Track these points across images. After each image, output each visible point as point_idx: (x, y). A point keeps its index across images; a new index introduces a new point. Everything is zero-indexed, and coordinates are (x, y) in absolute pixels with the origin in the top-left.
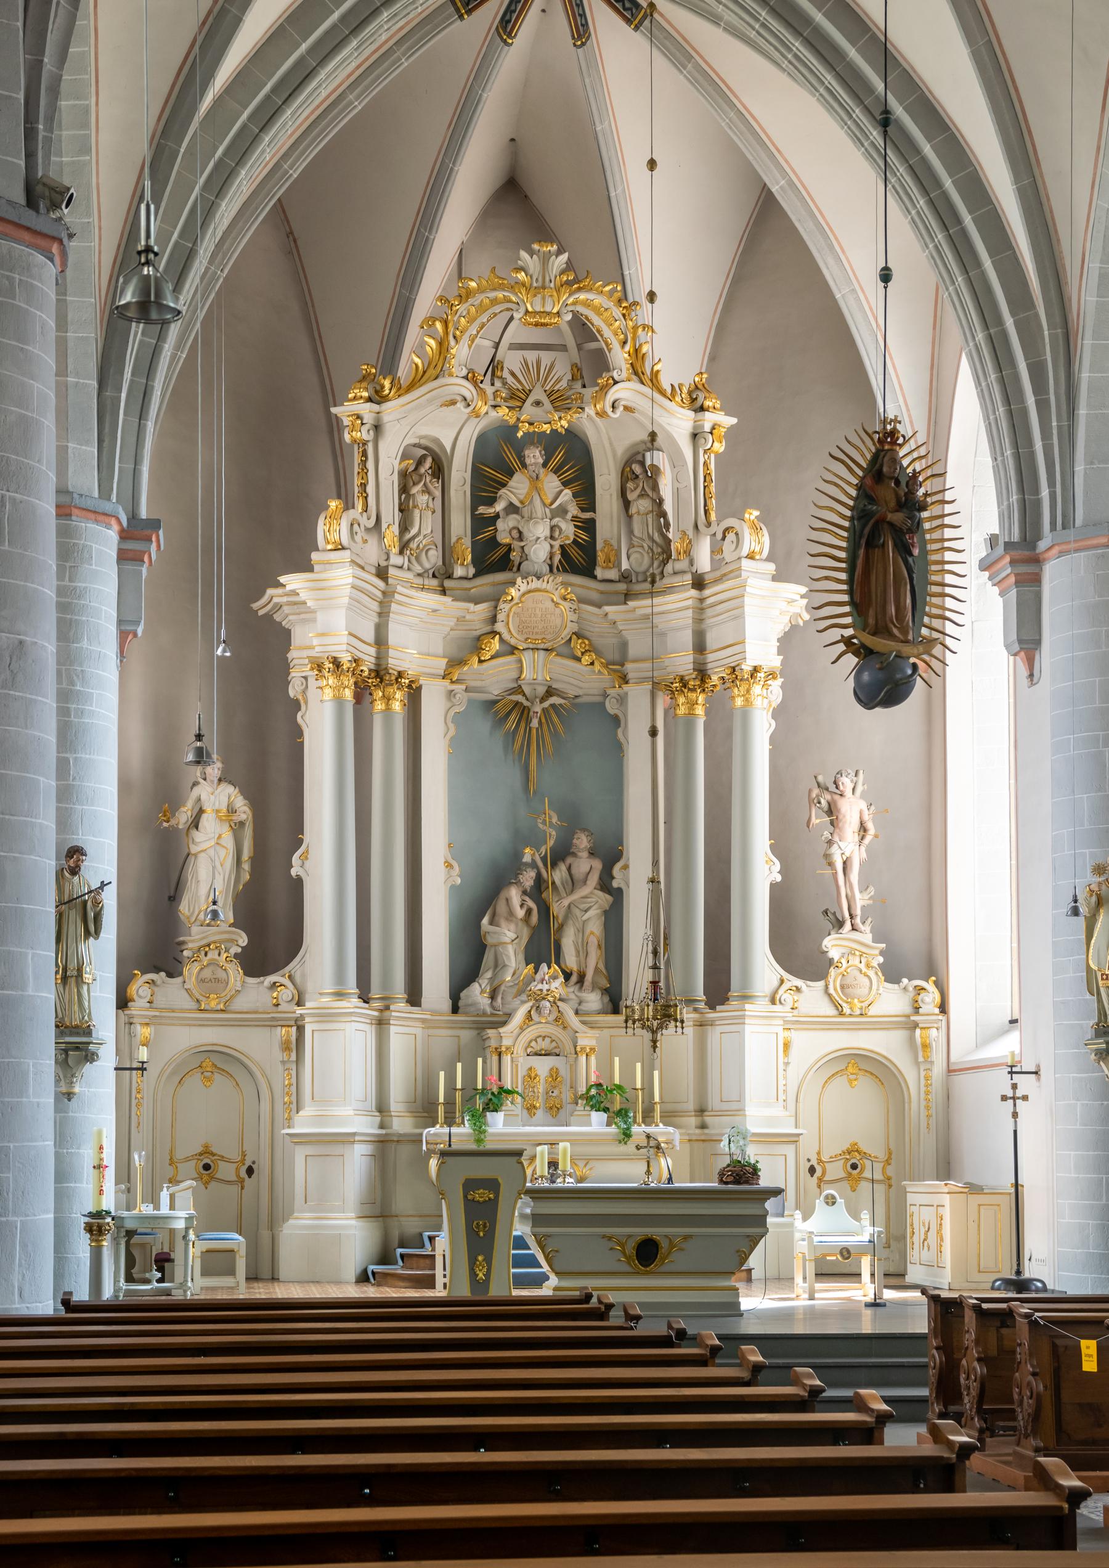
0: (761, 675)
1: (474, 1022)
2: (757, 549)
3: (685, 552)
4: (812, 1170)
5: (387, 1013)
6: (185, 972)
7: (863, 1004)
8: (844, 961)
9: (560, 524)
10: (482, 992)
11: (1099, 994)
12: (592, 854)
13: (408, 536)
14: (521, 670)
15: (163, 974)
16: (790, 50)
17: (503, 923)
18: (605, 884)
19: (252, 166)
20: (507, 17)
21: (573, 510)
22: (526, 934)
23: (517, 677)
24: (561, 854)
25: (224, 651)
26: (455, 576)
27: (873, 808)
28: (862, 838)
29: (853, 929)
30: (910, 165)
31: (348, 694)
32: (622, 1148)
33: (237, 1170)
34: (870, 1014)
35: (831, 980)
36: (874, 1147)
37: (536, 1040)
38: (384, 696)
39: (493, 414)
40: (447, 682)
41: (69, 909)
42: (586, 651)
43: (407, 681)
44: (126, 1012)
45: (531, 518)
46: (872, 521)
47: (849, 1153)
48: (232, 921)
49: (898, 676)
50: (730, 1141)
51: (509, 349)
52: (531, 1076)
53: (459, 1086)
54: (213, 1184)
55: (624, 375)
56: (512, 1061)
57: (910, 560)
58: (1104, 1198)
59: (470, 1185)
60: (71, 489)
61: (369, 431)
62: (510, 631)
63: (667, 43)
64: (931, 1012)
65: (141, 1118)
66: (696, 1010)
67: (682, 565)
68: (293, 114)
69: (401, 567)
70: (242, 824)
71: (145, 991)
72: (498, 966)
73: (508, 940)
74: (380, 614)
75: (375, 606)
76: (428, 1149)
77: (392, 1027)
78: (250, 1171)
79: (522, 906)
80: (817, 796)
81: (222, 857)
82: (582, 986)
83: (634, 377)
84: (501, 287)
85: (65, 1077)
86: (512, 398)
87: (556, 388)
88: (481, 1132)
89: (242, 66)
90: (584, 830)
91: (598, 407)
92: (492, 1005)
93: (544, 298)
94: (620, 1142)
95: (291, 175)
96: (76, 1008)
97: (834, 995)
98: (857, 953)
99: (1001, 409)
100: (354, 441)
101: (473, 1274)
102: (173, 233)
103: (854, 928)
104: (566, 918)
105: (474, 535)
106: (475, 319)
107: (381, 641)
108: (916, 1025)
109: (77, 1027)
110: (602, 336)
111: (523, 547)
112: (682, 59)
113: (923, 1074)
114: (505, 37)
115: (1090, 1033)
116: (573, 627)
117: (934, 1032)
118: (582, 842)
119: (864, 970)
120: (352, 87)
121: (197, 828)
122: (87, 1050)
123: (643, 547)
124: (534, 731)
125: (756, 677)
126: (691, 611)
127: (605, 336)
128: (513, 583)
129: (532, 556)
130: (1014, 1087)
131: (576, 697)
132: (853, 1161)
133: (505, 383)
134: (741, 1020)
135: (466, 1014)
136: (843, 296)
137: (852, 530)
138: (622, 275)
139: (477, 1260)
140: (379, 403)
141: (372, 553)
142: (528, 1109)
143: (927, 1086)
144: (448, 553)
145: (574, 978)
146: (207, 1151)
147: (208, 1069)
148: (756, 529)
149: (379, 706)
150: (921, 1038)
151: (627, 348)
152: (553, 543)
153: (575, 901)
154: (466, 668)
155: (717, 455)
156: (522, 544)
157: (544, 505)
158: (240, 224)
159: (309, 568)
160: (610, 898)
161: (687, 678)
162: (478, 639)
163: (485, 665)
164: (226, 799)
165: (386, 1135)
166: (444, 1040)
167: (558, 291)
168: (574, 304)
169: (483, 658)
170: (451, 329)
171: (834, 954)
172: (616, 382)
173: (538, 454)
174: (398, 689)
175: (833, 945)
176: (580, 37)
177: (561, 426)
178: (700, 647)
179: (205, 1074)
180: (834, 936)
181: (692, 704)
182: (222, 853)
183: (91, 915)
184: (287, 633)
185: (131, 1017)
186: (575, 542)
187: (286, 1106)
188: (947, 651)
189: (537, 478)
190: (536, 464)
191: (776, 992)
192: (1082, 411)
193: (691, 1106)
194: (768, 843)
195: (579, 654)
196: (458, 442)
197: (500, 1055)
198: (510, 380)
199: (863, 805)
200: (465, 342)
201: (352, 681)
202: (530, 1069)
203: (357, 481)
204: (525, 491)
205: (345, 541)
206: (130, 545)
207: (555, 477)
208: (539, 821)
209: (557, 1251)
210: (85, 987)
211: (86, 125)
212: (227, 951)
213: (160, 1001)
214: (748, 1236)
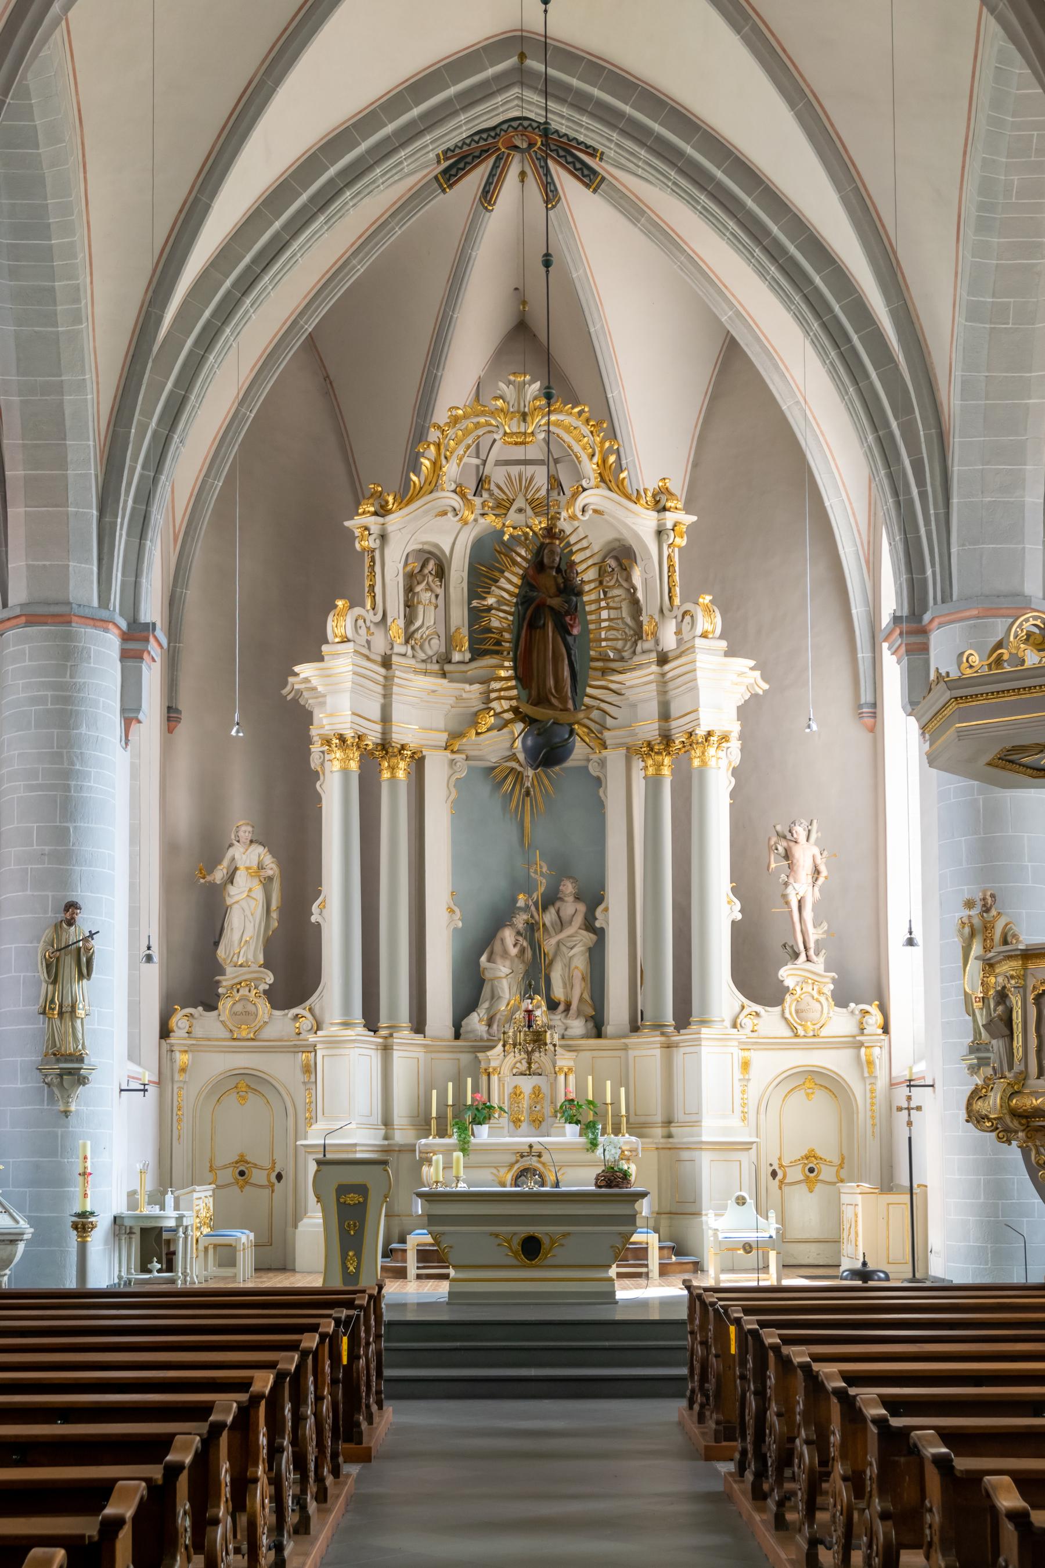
0: (714, 739)
1: (472, 1047)
2: (710, 629)
3: (652, 633)
4: (774, 1174)
5: (390, 1040)
6: (220, 1005)
7: (815, 1027)
8: (798, 989)
10: (480, 1020)
11: (974, 1015)
12: (578, 898)
13: (413, 628)
15: (200, 1008)
16: (698, 203)
17: (499, 960)
18: (589, 924)
19: (237, 325)
20: (487, 188)
22: (521, 968)
24: (550, 900)
25: (238, 732)
26: (453, 660)
27: (825, 853)
28: (816, 880)
29: (808, 960)
31: (354, 765)
32: (589, 1156)
33: (268, 1175)
34: (822, 1034)
35: (787, 1005)
36: (828, 1151)
37: (520, 1062)
38: (389, 766)
39: (481, 520)
40: (448, 753)
41: (65, 955)
43: (409, 753)
44: (168, 1041)
46: (533, 606)
47: (807, 1159)
48: (262, 962)
49: (557, 740)
50: (604, 1150)
51: (495, 465)
52: (516, 1093)
53: (450, 1102)
54: (248, 1188)
55: (593, 483)
56: (499, 1080)
57: (570, 639)
58: (982, 1196)
59: (342, 1190)
60: (71, 600)
63: (622, 202)
64: (874, 1033)
65: (181, 1132)
66: (663, 1034)
67: (649, 645)
68: (271, 280)
69: (404, 655)
70: (270, 879)
71: (184, 1024)
72: (494, 997)
73: (503, 975)
74: (385, 696)
75: (379, 689)
76: (420, 1158)
77: (395, 1052)
78: (279, 1177)
79: (515, 945)
80: (775, 843)
81: (252, 907)
82: (567, 1016)
83: (602, 484)
84: (483, 413)
85: (62, 1097)
86: (498, 506)
87: (536, 497)
88: (465, 1143)
89: (225, 242)
90: (569, 877)
91: (570, 511)
92: (488, 1032)
94: (588, 1150)
95: (307, 329)
96: (71, 1039)
97: (790, 1018)
98: (810, 981)
99: (891, 500)
101: (345, 1267)
102: (166, 384)
103: (808, 960)
104: (555, 955)
106: (461, 441)
107: (386, 719)
108: (861, 1044)
109: (70, 1055)
110: (572, 450)
112: (636, 214)
113: (868, 1087)
115: (965, 1050)
117: (876, 1051)
118: (568, 888)
119: (816, 996)
120: (355, 254)
121: (232, 883)
122: (79, 1075)
127: (575, 451)
130: (909, 1098)
132: (811, 1165)
133: (491, 495)
134: (697, 1042)
135: (466, 1040)
136: (788, 407)
137: (516, 614)
138: (606, 397)
139: (348, 1255)
140: (383, 516)
141: (380, 645)
142: (514, 1122)
143: (871, 1098)
144: (450, 642)
145: (561, 1007)
146: (242, 1160)
147: (243, 1089)
148: (708, 611)
149: (386, 775)
150: (866, 1055)
151: (595, 460)
153: (562, 939)
154: (464, 740)
155: (681, 549)
158: (265, 372)
159: (321, 659)
160: (594, 937)
161: (653, 743)
162: (476, 714)
163: (482, 736)
164: (257, 858)
165: (389, 1145)
166: (445, 1063)
169: (479, 731)
170: (443, 451)
171: (789, 982)
172: (584, 490)
174: (402, 759)
175: (788, 975)
178: (665, 716)
179: (241, 1093)
180: (790, 966)
181: (659, 766)
182: (253, 903)
183: (84, 959)
184: (310, 714)
185: (172, 1045)
187: (307, 1120)
188: (608, 717)
191: (737, 1017)
192: (955, 500)
193: (659, 1118)
194: (730, 886)
197: (489, 1075)
198: (496, 491)
199: (816, 851)
200: (454, 461)
201: (357, 754)
202: (516, 1087)
203: (367, 583)
205: (350, 635)
206: (131, 646)
209: (451, 1247)
210: (79, 1021)
211: (77, 300)
212: (256, 987)
213: (198, 1032)
214: (620, 1234)
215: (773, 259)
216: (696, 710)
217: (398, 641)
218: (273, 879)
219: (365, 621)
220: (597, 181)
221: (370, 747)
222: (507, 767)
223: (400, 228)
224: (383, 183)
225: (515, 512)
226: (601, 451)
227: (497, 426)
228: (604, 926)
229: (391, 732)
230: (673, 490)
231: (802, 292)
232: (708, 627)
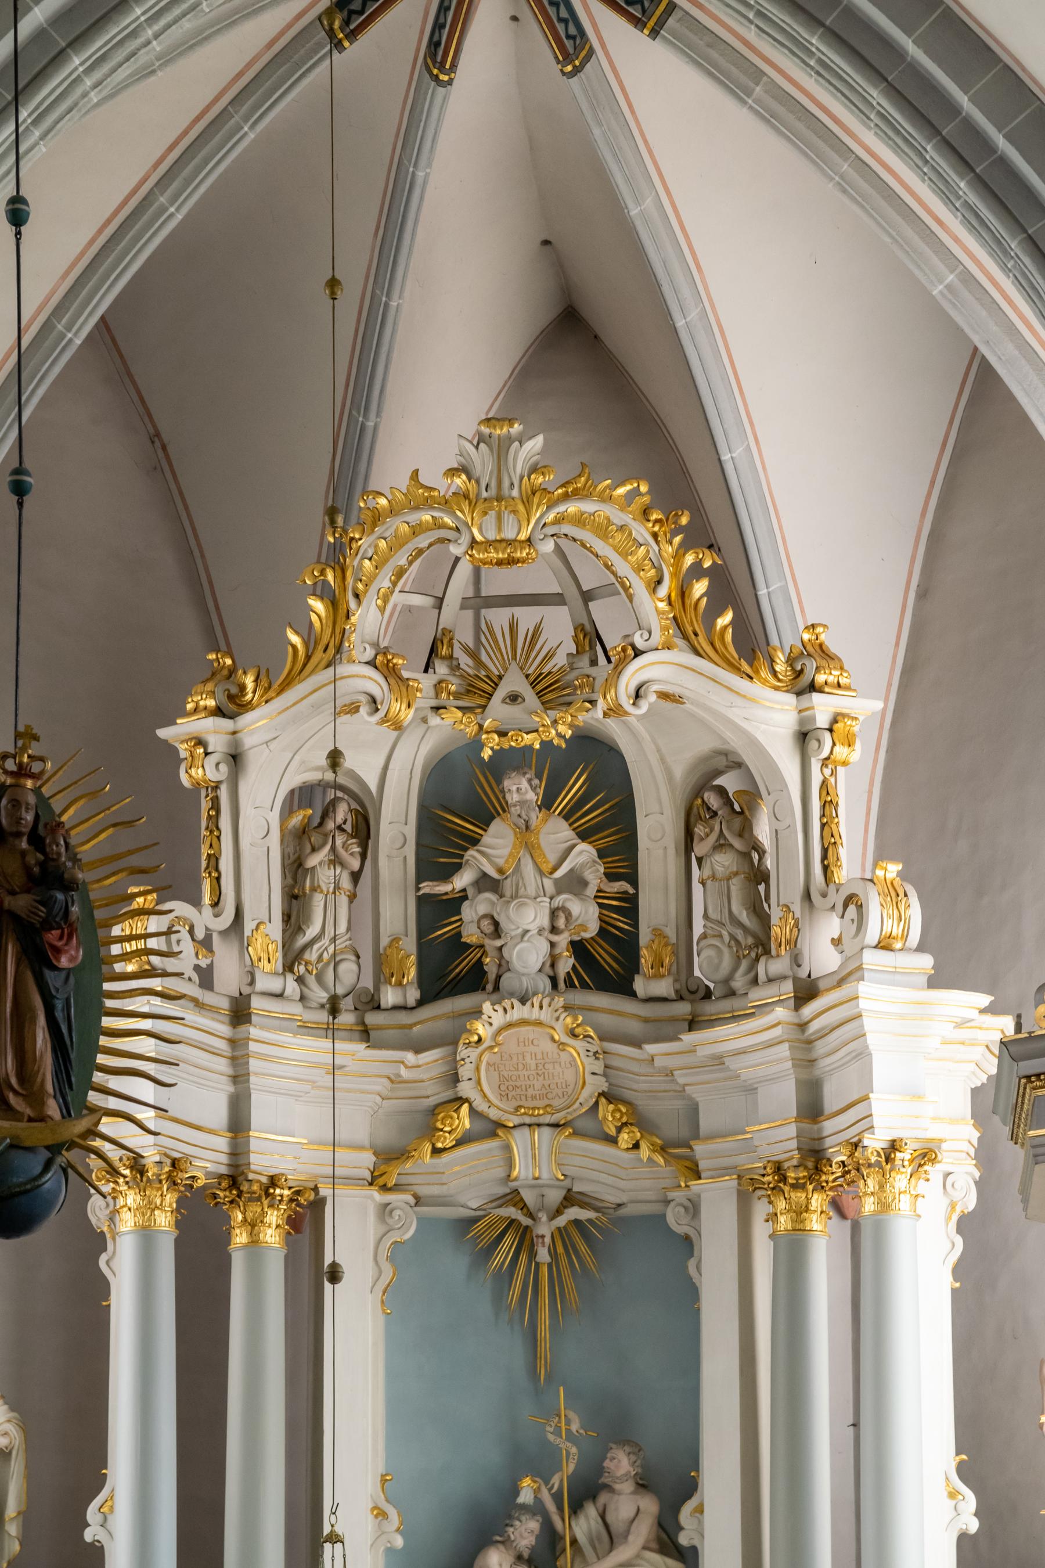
2: (897, 931)
3: (788, 942)
9: (569, 905)
12: (643, 1485)
13: (301, 941)
14: (510, 1163)
20: (436, 38)
21: (595, 877)
23: (503, 1175)
26: (383, 1005)
30: (1030, 237)
31: (164, 1220)
38: (245, 1220)
39: (434, 720)
42: (625, 1124)
43: (286, 1192)
45: (515, 896)
55: (657, 638)
57: (49, 975)
61: (217, 765)
62: (485, 1096)
63: (714, 54)
67: (778, 966)
69: (280, 996)
75: (222, 1065)
83: (680, 642)
86: (468, 691)
87: (545, 670)
93: (499, 519)
95: (71, 340)
100: (197, 785)
105: (421, 934)
111: (500, 949)
112: (743, 79)
114: (435, 71)
116: (596, 1085)
120: (163, 183)
123: (721, 936)
124: (545, 1270)
125: (894, 1159)
126: (786, 1045)
128: (477, 1013)
129: (516, 963)
131: (619, 1205)
133: (455, 668)
148: (893, 894)
149: (240, 1237)
151: (663, 591)
152: (555, 938)
154: (408, 1165)
156: (498, 943)
157: (541, 873)
162: (433, 1111)
163: (446, 1157)
167: (527, 503)
168: (557, 521)
169: (439, 1145)
170: (350, 580)
172: (638, 653)
173: (524, 784)
174: (271, 1206)
176: (567, 58)
177: (560, 735)
181: (800, 1212)
186: (602, 932)
189: (527, 827)
190: (522, 803)
195: (612, 1131)
196: (389, 773)
201: (171, 1199)
203: (205, 851)
204: (506, 852)
207: (564, 824)
208: (548, 1429)
215: (964, 164)
216: (866, 1098)
217: (268, 967)
218: (10, 1453)
219: (191, 932)
220: (658, 13)
221: (200, 1183)
222: (502, 1219)
223: (252, 127)
224: (156, 36)
225: (503, 701)
226: (674, 575)
227: (458, 529)
228: (696, 1542)
229: (248, 1152)
230: (833, 648)
231: (1025, 231)
232: (892, 927)
